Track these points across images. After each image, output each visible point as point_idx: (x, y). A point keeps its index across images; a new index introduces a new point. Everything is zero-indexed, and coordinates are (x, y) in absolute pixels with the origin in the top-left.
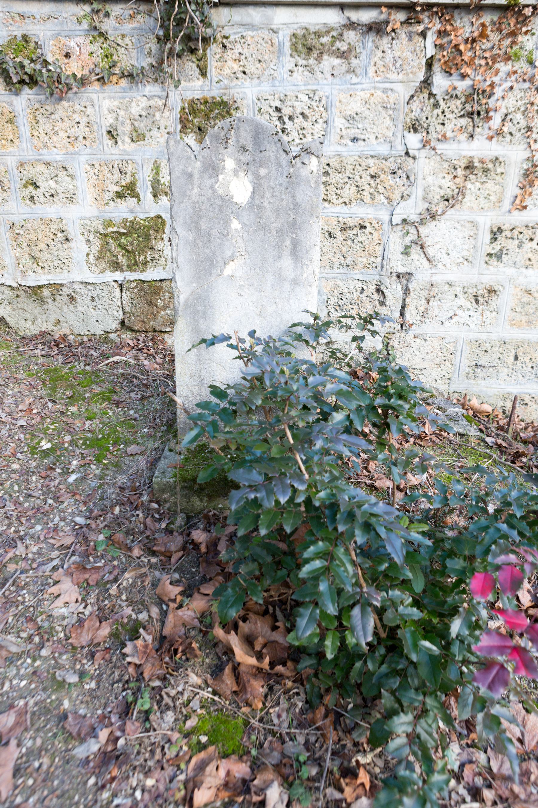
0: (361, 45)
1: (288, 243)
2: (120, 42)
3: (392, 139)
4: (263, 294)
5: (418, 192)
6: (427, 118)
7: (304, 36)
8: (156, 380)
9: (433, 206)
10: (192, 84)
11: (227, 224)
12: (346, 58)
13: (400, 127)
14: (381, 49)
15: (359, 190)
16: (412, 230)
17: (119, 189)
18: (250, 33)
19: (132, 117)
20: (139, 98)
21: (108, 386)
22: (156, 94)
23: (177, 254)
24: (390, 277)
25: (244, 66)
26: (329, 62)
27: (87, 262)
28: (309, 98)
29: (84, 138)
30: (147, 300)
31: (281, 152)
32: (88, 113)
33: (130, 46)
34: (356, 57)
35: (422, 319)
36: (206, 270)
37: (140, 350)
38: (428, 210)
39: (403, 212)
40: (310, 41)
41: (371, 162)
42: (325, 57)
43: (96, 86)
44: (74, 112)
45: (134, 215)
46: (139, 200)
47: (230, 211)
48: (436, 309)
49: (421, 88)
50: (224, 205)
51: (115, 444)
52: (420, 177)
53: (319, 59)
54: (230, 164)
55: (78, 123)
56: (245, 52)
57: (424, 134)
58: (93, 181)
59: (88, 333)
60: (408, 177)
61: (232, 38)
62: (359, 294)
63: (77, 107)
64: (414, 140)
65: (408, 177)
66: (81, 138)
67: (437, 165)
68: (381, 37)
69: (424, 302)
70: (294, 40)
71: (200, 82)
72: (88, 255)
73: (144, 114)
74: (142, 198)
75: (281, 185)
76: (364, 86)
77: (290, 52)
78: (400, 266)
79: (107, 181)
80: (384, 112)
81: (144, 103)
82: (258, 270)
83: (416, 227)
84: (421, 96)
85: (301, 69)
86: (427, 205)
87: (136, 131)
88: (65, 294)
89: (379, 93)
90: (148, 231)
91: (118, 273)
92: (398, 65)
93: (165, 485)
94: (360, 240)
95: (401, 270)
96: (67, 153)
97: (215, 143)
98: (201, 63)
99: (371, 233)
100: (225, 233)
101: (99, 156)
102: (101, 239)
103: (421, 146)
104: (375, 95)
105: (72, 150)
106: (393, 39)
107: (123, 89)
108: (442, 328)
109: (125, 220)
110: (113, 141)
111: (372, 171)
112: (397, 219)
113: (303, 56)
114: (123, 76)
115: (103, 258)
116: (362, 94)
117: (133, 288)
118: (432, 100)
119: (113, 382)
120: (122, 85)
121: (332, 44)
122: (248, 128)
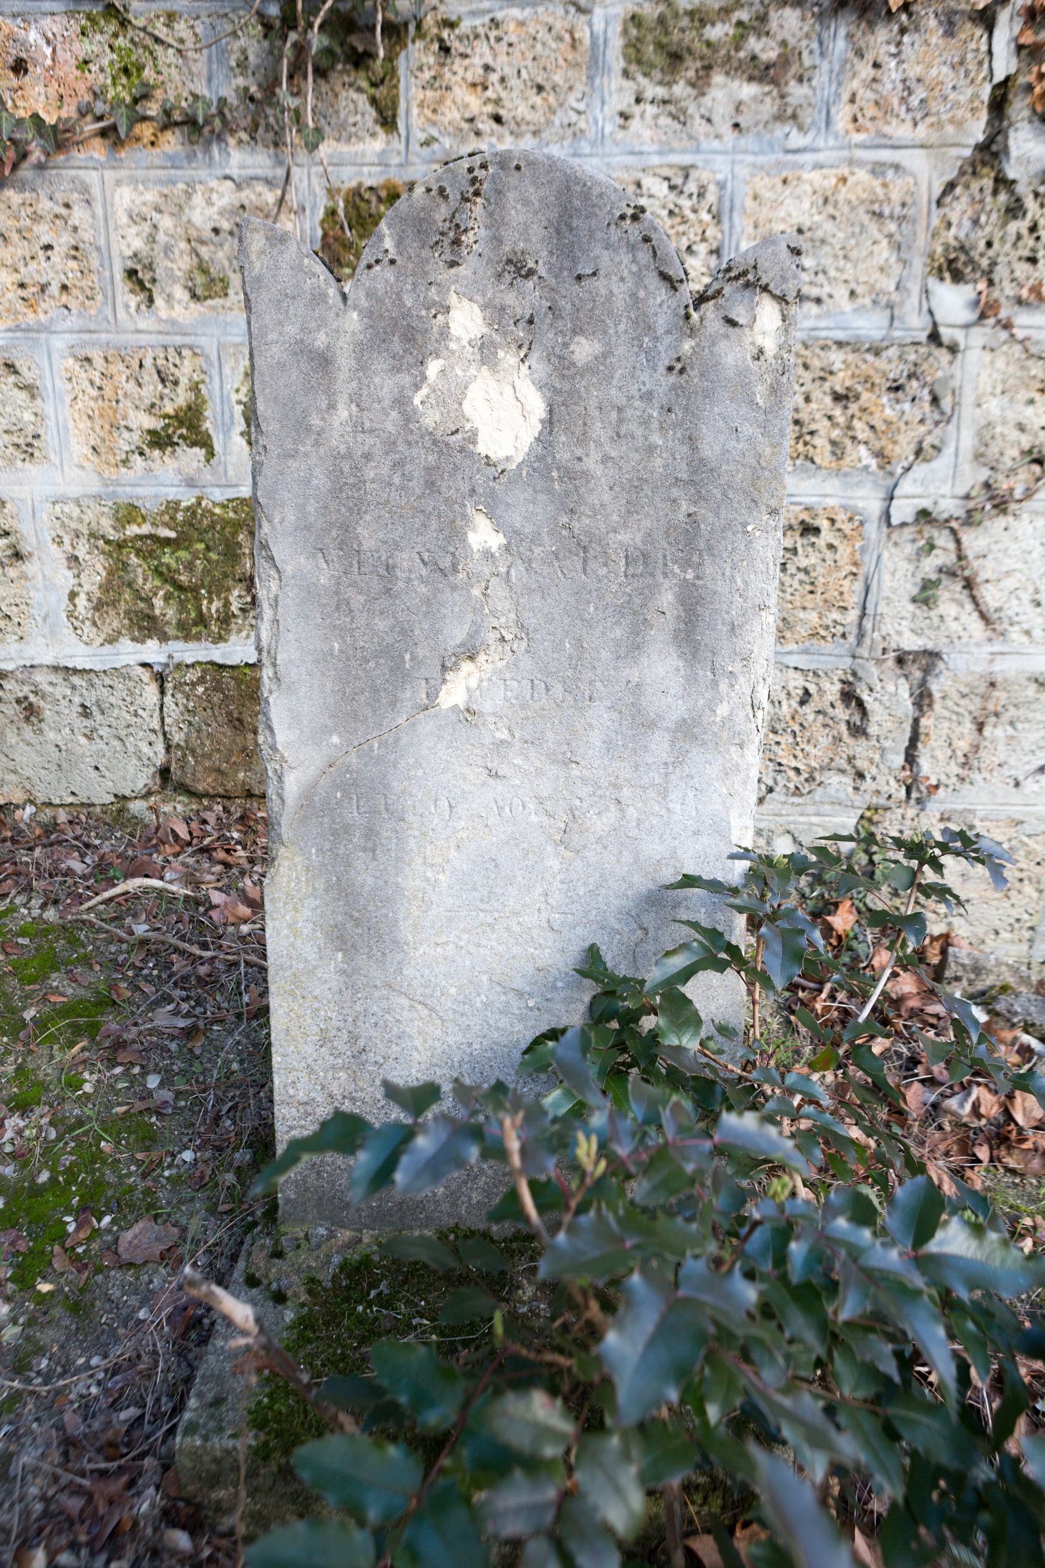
0: (815, 45)
1: (667, 599)
2: (161, 32)
3: (895, 297)
4: (575, 771)
5: (963, 438)
6: (989, 244)
7: (661, 20)
8: (235, 964)
9: (1001, 477)
10: (357, 147)
11: (454, 532)
12: (774, 82)
13: (918, 264)
14: (870, 57)
15: (803, 430)
16: (943, 540)
17: (157, 424)
18: (515, 12)
19: (193, 233)
20: (214, 184)
21: (97, 976)
22: (259, 172)
23: (276, 635)
24: (879, 662)
25: (498, 102)
26: (728, 91)
27: (70, 615)
28: (672, 188)
29: (64, 288)
30: (229, 714)
31: (653, 281)
32: (74, 221)
33: (189, 44)
34: (800, 80)
35: (964, 773)
36: (375, 690)
37: (206, 850)
38: (987, 485)
39: (919, 490)
40: (676, 36)
41: (836, 358)
42: (718, 78)
43: (98, 151)
44: (36, 218)
45: (197, 492)
46: (211, 454)
47: (465, 488)
48: (1001, 747)
49: (973, 164)
50: (448, 461)
51: (86, 1211)
52: (968, 399)
53: (700, 84)
54: (466, 321)
55: (48, 247)
56: (503, 64)
57: (982, 286)
58: (86, 403)
59: (70, 799)
60: (935, 400)
61: (465, 26)
62: (794, 704)
63: (45, 206)
64: (953, 302)
65: (935, 400)
66: (54, 289)
67: (1012, 369)
68: (871, 25)
69: (968, 726)
70: (634, 32)
71: (377, 144)
72: (73, 595)
73: (225, 225)
74: (217, 447)
75: (647, 397)
76: (821, 157)
77: (622, 63)
78: (908, 634)
79: (126, 404)
80: (873, 228)
81: (226, 196)
82: (558, 689)
83: (953, 532)
84: (975, 186)
85: (651, 110)
86: (984, 474)
87: (204, 270)
88: (11, 697)
89: (862, 175)
90: (234, 534)
91: (152, 644)
92: (914, 101)
93: (216, 1460)
94: (802, 565)
95: (911, 643)
96: (18, 328)
97: (413, 247)
98: (380, 92)
99: (831, 546)
100: (446, 562)
101: (104, 337)
102: (109, 554)
103: (973, 316)
104: (851, 180)
105: (30, 318)
106: (903, 31)
107: (170, 158)
108: (1015, 796)
109: (173, 506)
110: (142, 296)
111: (840, 382)
112: (903, 511)
113: (657, 75)
114: (168, 123)
115: (114, 603)
116: (815, 176)
117: (193, 685)
118: (1003, 197)
119: (118, 966)
120: (168, 149)
121: (738, 42)
122: (533, 193)
